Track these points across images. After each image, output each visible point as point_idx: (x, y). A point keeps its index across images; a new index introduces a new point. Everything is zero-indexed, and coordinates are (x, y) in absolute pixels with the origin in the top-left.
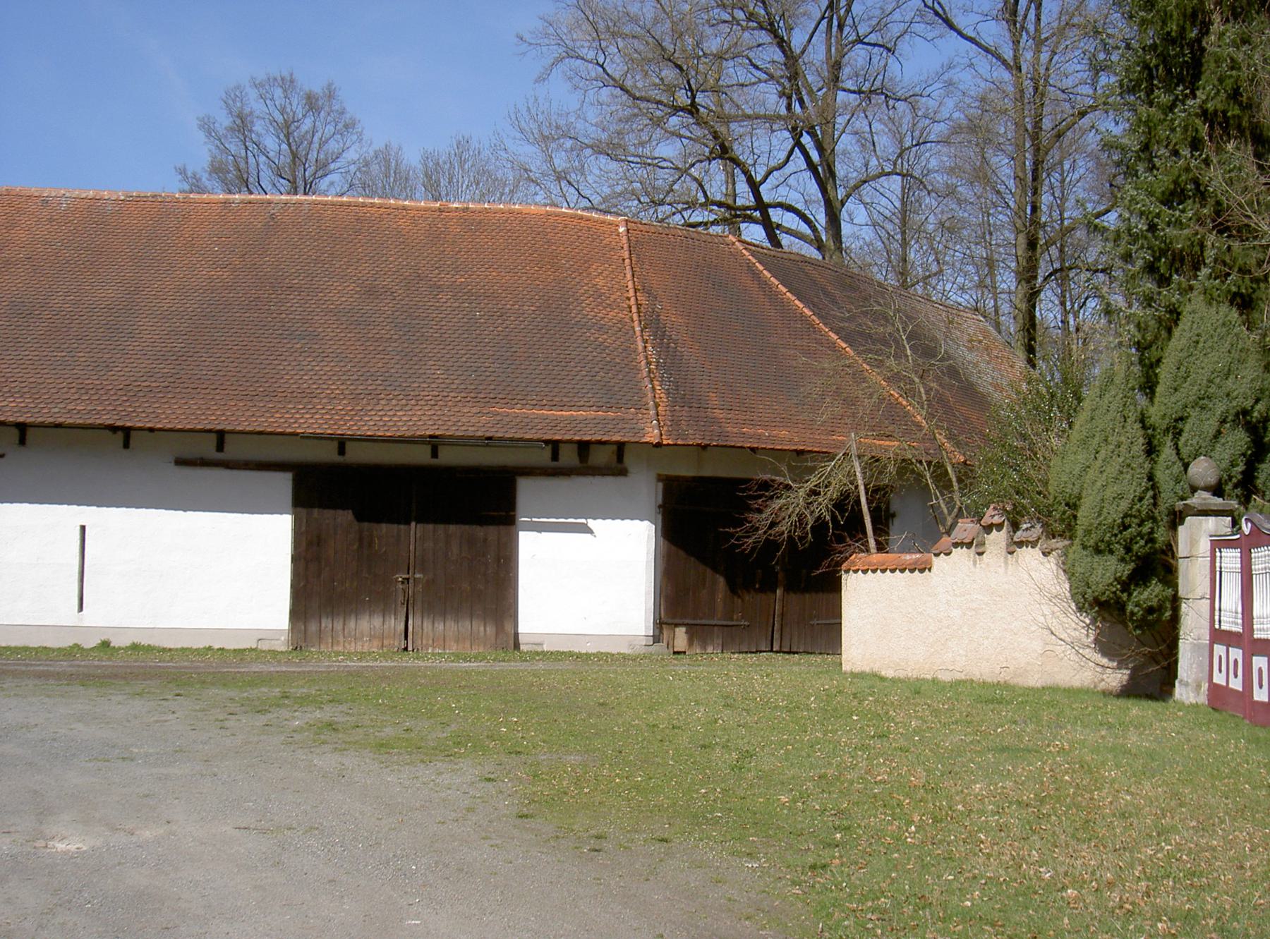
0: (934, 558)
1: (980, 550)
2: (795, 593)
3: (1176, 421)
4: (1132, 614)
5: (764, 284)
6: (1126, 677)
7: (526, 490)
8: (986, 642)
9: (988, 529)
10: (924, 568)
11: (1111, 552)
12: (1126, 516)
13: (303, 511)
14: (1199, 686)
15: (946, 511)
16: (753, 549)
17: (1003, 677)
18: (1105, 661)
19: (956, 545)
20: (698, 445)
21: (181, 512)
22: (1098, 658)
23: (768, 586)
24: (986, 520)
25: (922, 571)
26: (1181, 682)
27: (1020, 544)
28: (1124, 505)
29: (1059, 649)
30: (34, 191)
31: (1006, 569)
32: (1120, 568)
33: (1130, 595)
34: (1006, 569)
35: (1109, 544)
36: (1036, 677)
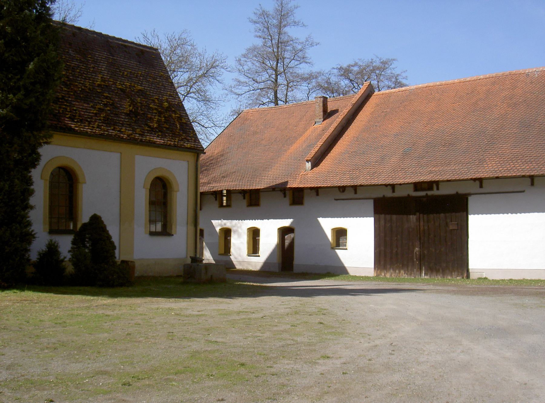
7: (472, 202)
13: (377, 216)
21: (502, 215)
30: (521, 71)
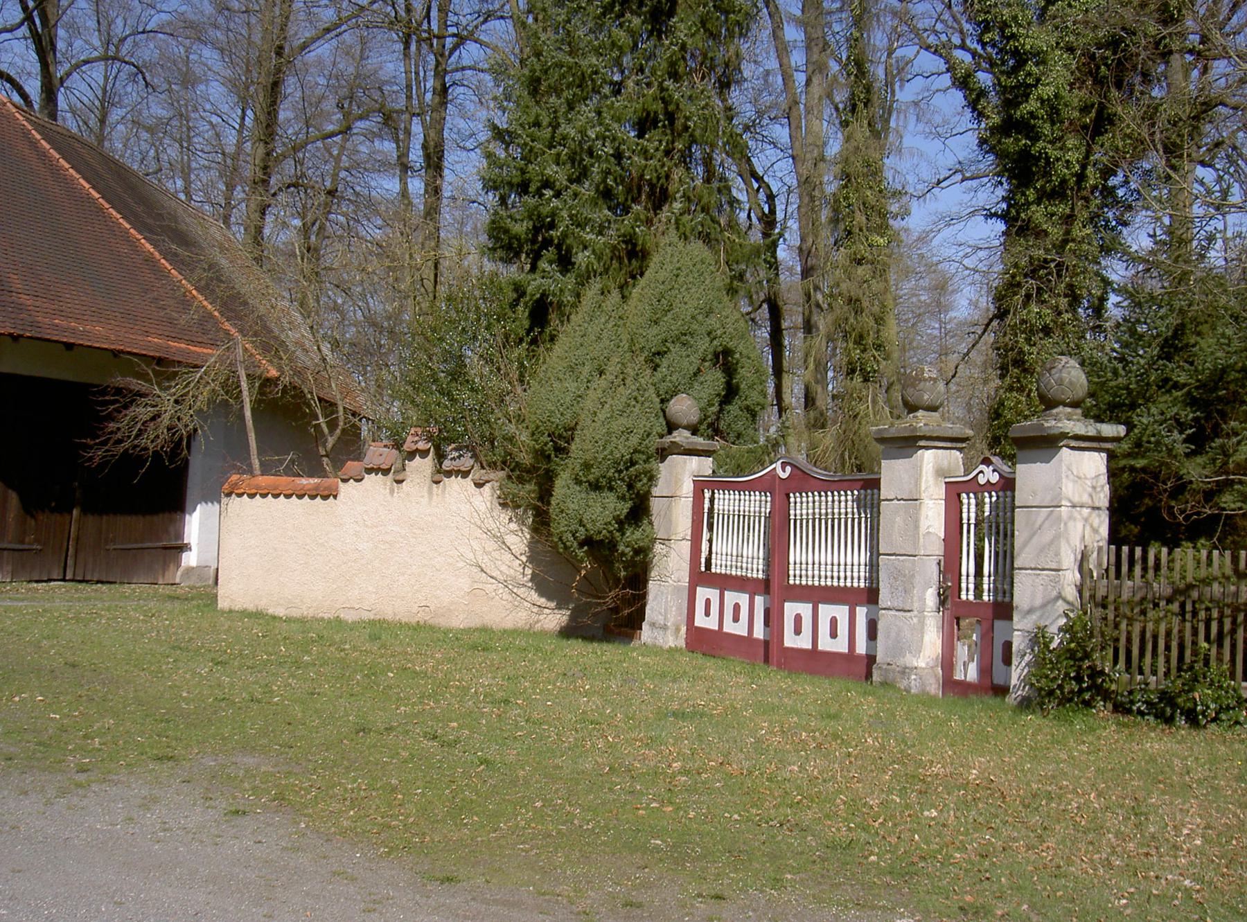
0: (341, 484)
1: (400, 477)
2: (93, 514)
3: (654, 354)
4: (623, 554)
5: (44, 155)
6: (565, 619)
8: (401, 578)
9: (411, 455)
10: (329, 494)
11: (611, 489)
12: (636, 451)
14: (678, 630)
15: (326, 430)
16: (102, 465)
17: (422, 617)
18: (543, 601)
19: (369, 471)
20: (11, 335)
22: (534, 596)
23: (64, 508)
24: (409, 446)
25: (325, 498)
26: (653, 625)
27: (449, 474)
28: (634, 440)
29: (489, 588)
31: (430, 498)
32: (619, 506)
33: (623, 534)
34: (430, 498)
35: (610, 480)
36: (461, 617)
